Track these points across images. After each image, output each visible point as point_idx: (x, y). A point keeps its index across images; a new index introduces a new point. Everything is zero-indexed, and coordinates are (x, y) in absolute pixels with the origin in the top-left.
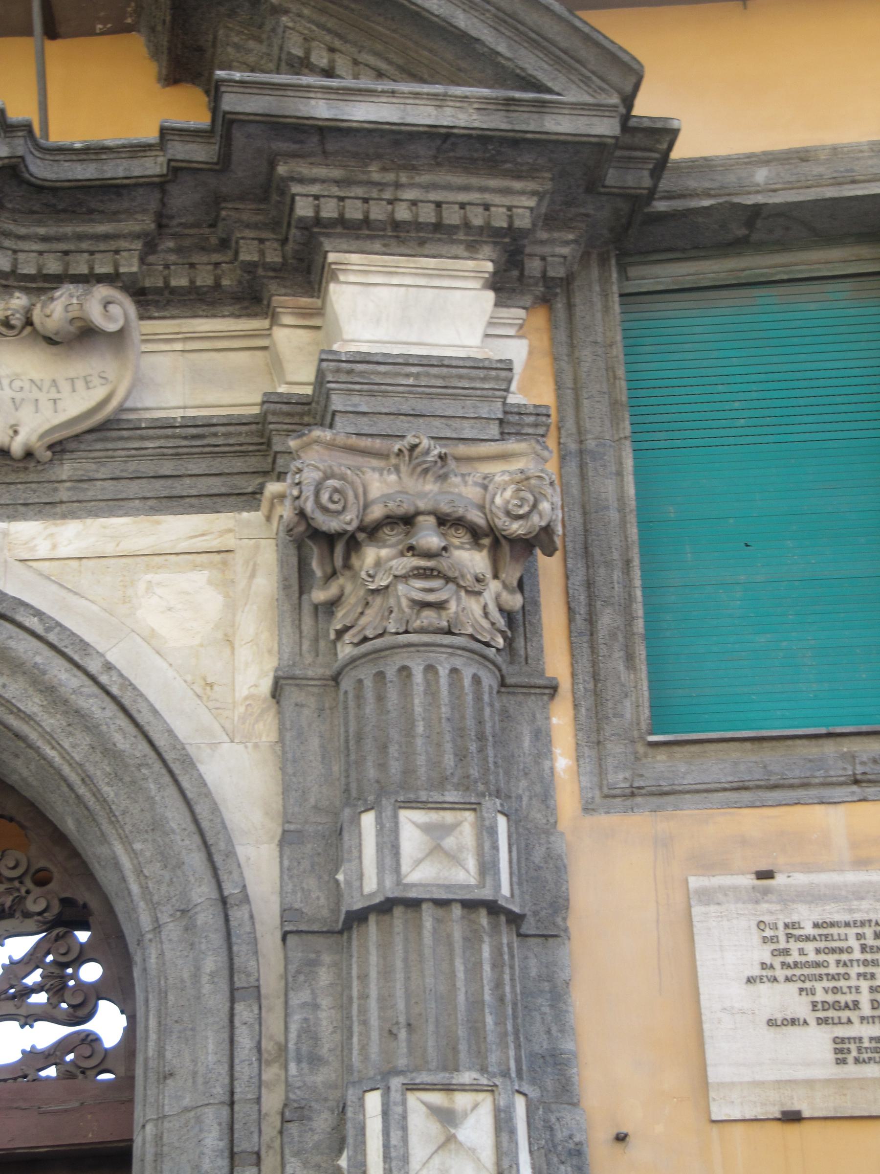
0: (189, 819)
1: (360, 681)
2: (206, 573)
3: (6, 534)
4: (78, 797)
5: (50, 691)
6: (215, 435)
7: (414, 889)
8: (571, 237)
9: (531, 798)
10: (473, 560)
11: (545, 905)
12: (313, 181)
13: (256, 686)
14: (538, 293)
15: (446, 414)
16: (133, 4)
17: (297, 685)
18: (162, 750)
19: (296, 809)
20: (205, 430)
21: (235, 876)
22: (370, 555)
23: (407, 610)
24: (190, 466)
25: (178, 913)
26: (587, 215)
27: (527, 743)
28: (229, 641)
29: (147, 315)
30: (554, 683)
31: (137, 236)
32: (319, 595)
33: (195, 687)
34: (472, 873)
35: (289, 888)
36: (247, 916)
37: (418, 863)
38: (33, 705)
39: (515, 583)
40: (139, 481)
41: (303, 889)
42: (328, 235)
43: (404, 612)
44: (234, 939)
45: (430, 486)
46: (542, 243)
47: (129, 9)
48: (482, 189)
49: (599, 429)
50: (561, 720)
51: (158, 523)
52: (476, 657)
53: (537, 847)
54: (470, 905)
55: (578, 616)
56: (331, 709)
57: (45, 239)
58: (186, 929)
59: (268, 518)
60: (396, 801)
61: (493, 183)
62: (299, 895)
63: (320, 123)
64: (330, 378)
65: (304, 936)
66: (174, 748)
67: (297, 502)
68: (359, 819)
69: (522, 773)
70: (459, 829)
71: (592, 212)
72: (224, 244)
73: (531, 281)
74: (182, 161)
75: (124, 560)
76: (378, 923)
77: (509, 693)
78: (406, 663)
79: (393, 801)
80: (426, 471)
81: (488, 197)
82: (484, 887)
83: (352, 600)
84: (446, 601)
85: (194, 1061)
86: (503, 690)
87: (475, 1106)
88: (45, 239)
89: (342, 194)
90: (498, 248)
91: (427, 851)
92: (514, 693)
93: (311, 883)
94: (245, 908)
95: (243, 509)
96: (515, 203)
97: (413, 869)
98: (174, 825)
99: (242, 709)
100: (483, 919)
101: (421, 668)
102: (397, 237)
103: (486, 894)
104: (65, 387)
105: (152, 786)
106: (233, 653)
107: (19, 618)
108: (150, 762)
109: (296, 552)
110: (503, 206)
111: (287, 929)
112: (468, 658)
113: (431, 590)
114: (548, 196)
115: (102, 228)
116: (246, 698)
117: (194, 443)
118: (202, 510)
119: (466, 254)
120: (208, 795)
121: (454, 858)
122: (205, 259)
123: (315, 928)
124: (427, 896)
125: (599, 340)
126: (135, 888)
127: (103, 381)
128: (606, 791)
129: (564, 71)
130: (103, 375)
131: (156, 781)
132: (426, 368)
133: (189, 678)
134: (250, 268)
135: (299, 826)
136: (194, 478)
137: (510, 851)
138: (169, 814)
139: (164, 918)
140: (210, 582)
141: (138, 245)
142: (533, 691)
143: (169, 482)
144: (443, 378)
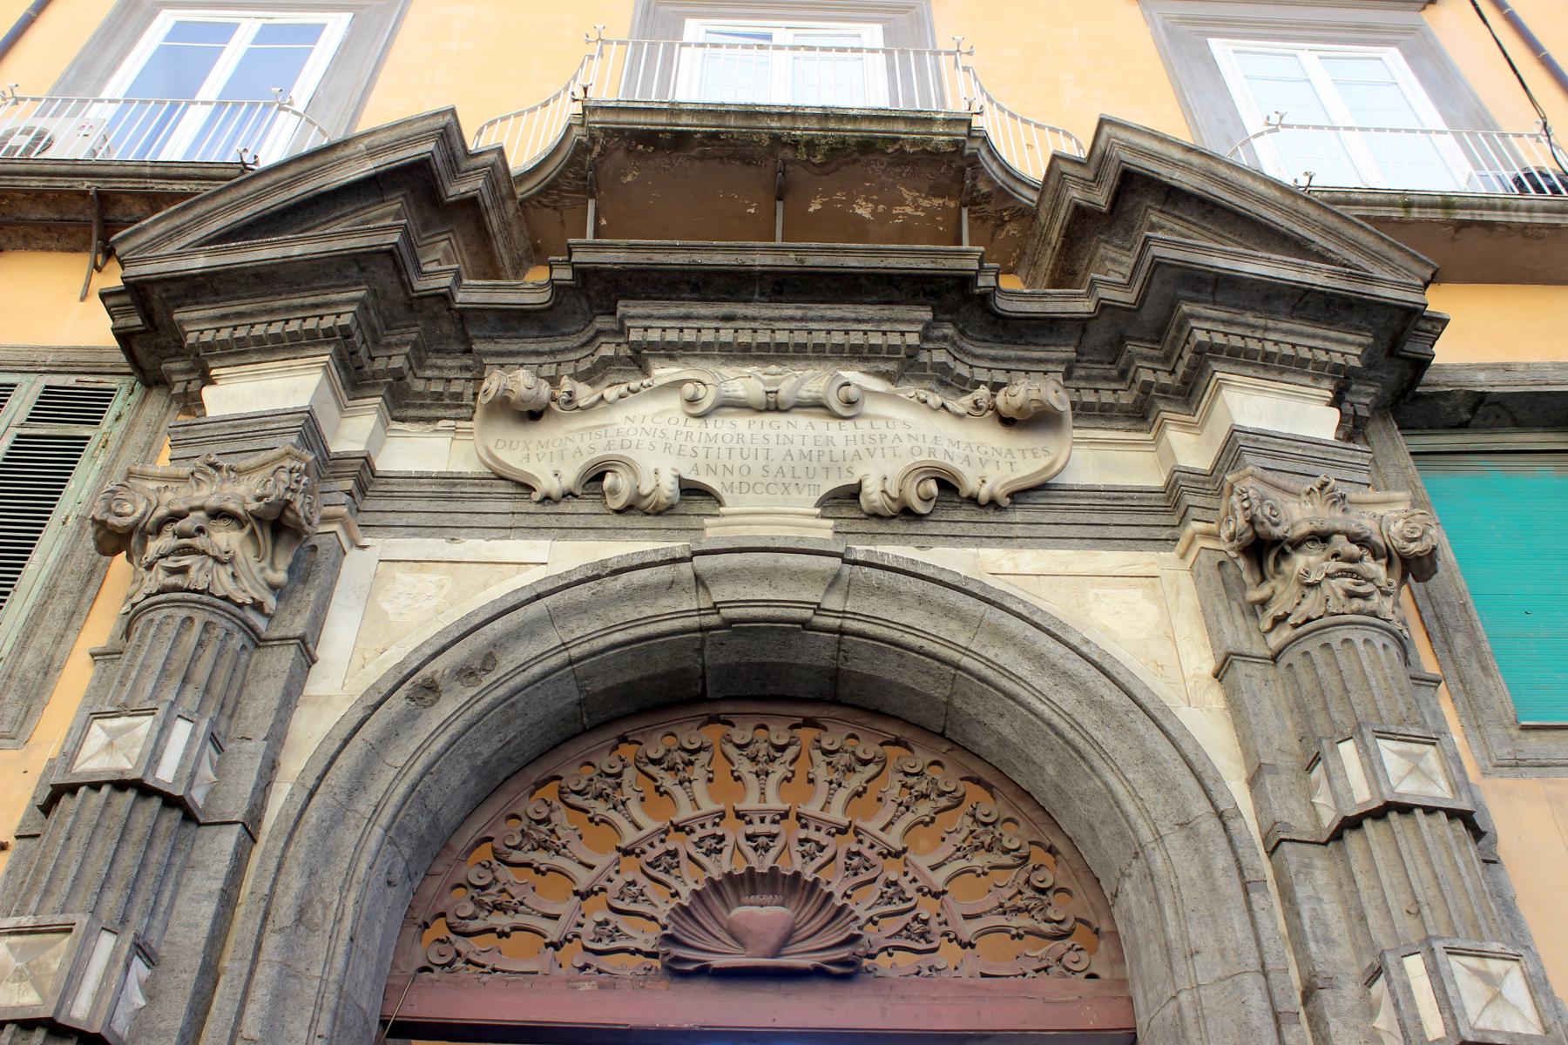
1: (1306, 653)
3: (977, 556)
4: (1067, 742)
5: (1039, 659)
8: (1372, 390)
12: (1207, 319)
22: (1300, 561)
31: (1062, 362)
37: (1402, 779)
38: (1023, 669)
42: (1216, 359)
48: (1325, 339)
57: (994, 359)
58: (1188, 838)
61: (1333, 334)
72: (1122, 375)
81: (1328, 345)
84: (1371, 593)
85: (1220, 940)
87: (1507, 972)
88: (994, 359)
104: (1018, 455)
107: (1007, 604)
118: (1128, 549)
120: (1189, 735)
121: (1428, 776)
122: (1106, 386)
123: (1305, 838)
126: (1131, 808)
128: (1495, 761)
134: (1147, 386)
138: (1159, 748)
139: (1163, 831)
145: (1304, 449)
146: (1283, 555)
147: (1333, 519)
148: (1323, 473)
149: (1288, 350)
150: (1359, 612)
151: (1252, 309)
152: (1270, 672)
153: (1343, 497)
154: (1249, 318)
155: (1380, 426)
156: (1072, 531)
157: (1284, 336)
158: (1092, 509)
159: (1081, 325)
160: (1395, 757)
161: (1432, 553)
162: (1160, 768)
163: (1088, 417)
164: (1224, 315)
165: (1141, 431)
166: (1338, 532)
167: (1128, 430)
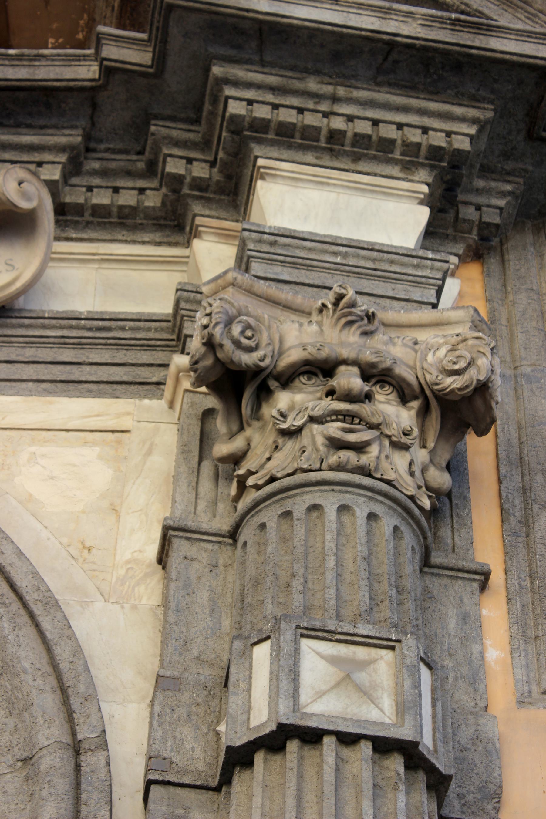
0: (45, 659)
2: (97, 449)
6: (123, 329)
7: (314, 718)
8: (508, 188)
9: (456, 679)
10: (401, 417)
11: (472, 789)
12: (249, 85)
13: (140, 551)
14: (471, 242)
15: (375, 292)
16: (85, 16)
17: (188, 539)
18: (23, 592)
19: (176, 658)
20: (113, 324)
21: (94, 720)
22: (283, 399)
23: (322, 448)
24: (91, 356)
25: (20, 764)
26: (526, 171)
27: (452, 624)
28: (115, 510)
29: (64, 235)
30: (485, 568)
31: (62, 149)
32: (222, 449)
33: (70, 549)
34: (388, 714)
35: (159, 734)
36: (103, 762)
37: (321, 694)
39: (444, 465)
40: (35, 366)
41: (175, 738)
42: (260, 141)
43: (317, 450)
44: (83, 786)
45: (352, 337)
46: (479, 192)
47: (82, 22)
48: (422, 112)
49: (535, 358)
50: (494, 612)
51: (50, 403)
52: (399, 509)
53: (463, 727)
54: (383, 746)
55: (512, 518)
56: (225, 566)
59: (171, 405)
60: (298, 627)
61: (433, 106)
62: (170, 743)
63: (261, 17)
64: (251, 246)
65: (172, 789)
66: (38, 589)
67: (206, 331)
68: (251, 651)
69: (445, 654)
70: (372, 666)
71: (530, 168)
73: (466, 226)
74: (116, 61)
75: (8, 432)
76: (265, 761)
77: (433, 574)
78: (318, 502)
79: (294, 626)
80: (350, 323)
81: (427, 121)
82: (402, 726)
83: (259, 451)
84: (368, 443)
86: (426, 569)
89: (277, 101)
90: (435, 173)
91: (333, 683)
92: (438, 575)
93: (186, 732)
94: (101, 755)
95: (145, 397)
96: (455, 129)
97: (315, 700)
98: (27, 665)
99: (122, 572)
100: (396, 764)
101: (335, 507)
102: (331, 150)
103: (405, 733)
105: (6, 625)
106: (118, 521)
108: (7, 601)
109: (200, 424)
110: (441, 131)
111: (151, 777)
112: (390, 508)
113: (351, 431)
114: (489, 127)
115: (27, 139)
116: (128, 562)
117: (98, 335)
118: (100, 395)
119: (401, 175)
121: (367, 694)
122: (130, 184)
123: (186, 780)
124: (331, 727)
125: (535, 288)
127: (10, 268)
129: (510, 10)
130: (9, 262)
131: (12, 620)
132: (357, 250)
133: (65, 540)
135: (176, 674)
136: (95, 367)
137: (434, 706)
138: (22, 653)
140: (100, 457)
141: (63, 158)
142: (460, 575)
143: (68, 368)
144: (374, 260)
145: (345, 255)
146: (264, 393)
147: (342, 344)
148: (336, 283)
149: (364, 128)
150: (339, 467)
151: (317, 72)
152: (224, 555)
153: (370, 317)
154: (312, 84)
155: (529, 238)
156: (29, 371)
157: (358, 109)
158: (63, 342)
159: (87, 97)
160: (322, 665)
161: (483, 388)
162: (16, 682)
163: (102, 226)
164: (272, 80)
165: (176, 244)
166: (345, 362)
167: (159, 244)
